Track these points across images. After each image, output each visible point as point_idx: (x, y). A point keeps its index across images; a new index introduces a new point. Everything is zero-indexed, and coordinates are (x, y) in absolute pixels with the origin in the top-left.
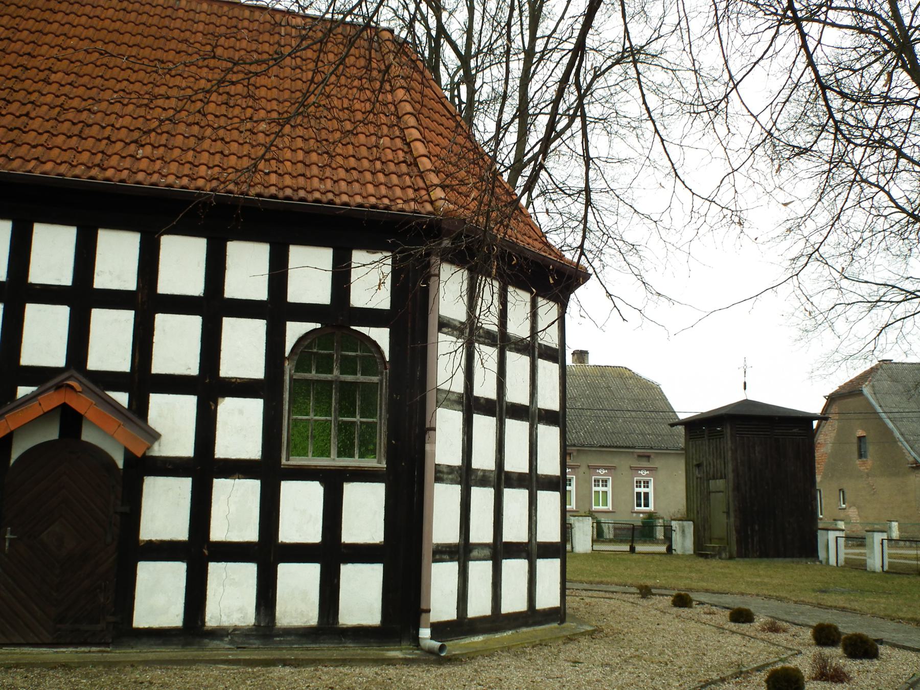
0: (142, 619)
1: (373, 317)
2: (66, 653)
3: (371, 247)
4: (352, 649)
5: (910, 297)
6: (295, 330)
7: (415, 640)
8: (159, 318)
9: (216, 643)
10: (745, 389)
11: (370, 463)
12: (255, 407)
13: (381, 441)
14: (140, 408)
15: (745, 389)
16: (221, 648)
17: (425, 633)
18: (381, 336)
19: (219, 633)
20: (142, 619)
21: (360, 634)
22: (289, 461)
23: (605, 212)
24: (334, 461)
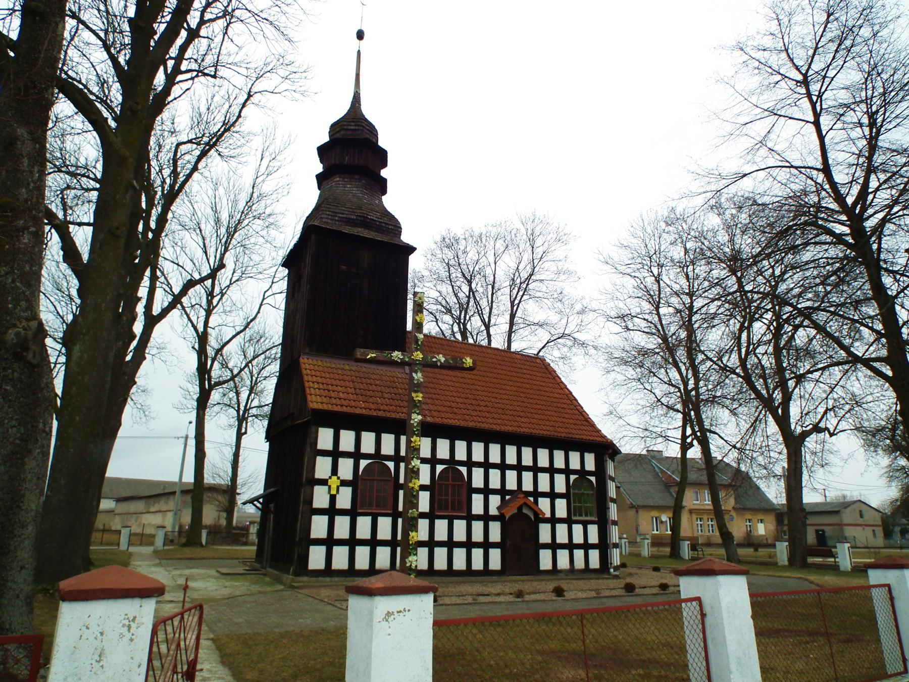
0: (542, 567)
1: (591, 473)
2: (525, 577)
3: (590, 452)
4: (593, 576)
5: (162, 279)
6: (573, 477)
7: (609, 573)
8: (335, 537)
9: (560, 574)
10: (359, 52)
11: (593, 519)
12: (564, 501)
13: (595, 511)
14: (536, 502)
15: (359, 52)
16: (561, 575)
17: (612, 570)
18: (593, 479)
19: (561, 571)
20: (542, 567)
21: (595, 571)
22: (574, 518)
23: (224, 217)
24: (583, 518)
